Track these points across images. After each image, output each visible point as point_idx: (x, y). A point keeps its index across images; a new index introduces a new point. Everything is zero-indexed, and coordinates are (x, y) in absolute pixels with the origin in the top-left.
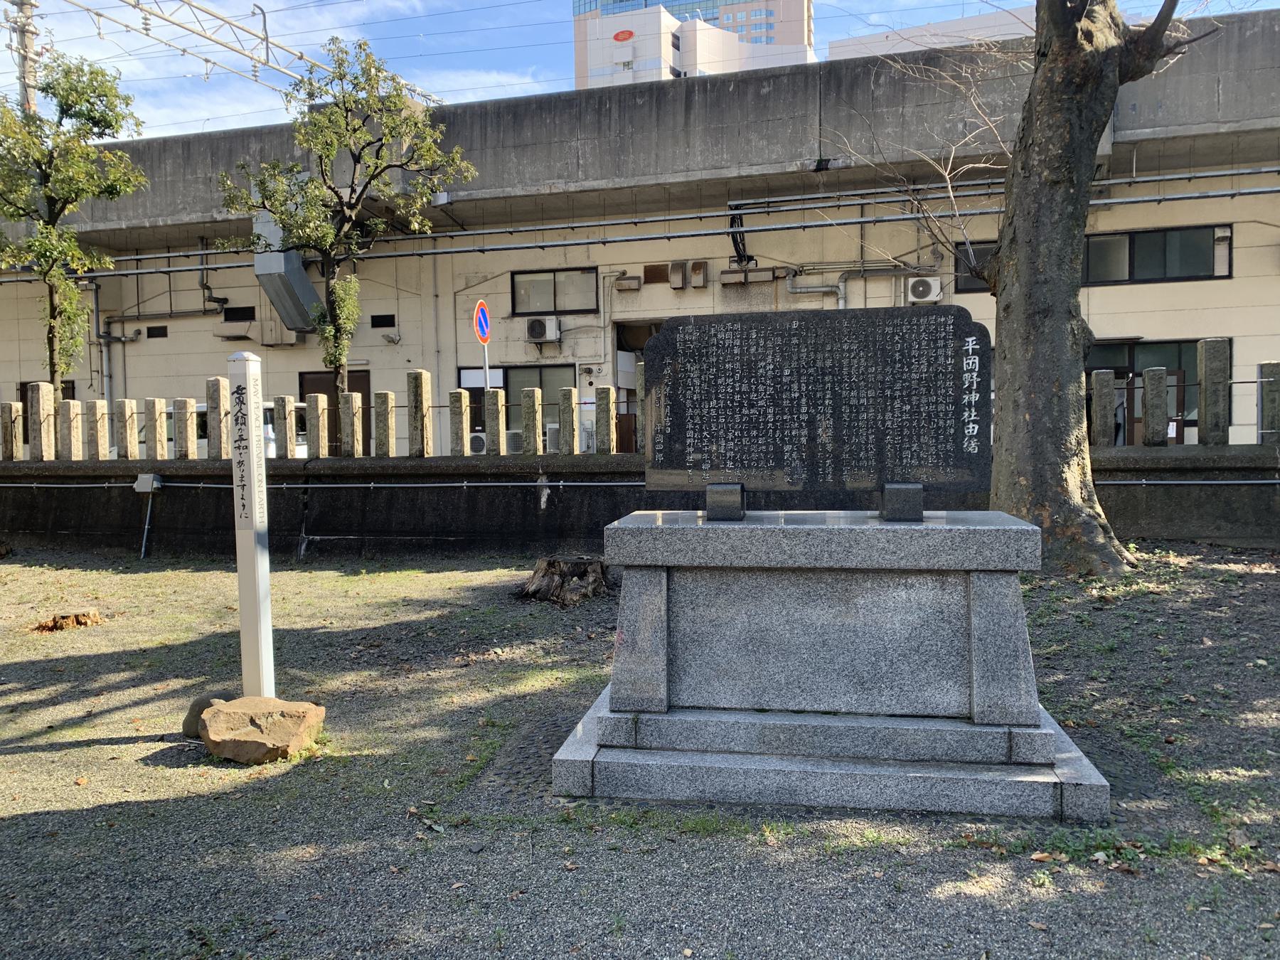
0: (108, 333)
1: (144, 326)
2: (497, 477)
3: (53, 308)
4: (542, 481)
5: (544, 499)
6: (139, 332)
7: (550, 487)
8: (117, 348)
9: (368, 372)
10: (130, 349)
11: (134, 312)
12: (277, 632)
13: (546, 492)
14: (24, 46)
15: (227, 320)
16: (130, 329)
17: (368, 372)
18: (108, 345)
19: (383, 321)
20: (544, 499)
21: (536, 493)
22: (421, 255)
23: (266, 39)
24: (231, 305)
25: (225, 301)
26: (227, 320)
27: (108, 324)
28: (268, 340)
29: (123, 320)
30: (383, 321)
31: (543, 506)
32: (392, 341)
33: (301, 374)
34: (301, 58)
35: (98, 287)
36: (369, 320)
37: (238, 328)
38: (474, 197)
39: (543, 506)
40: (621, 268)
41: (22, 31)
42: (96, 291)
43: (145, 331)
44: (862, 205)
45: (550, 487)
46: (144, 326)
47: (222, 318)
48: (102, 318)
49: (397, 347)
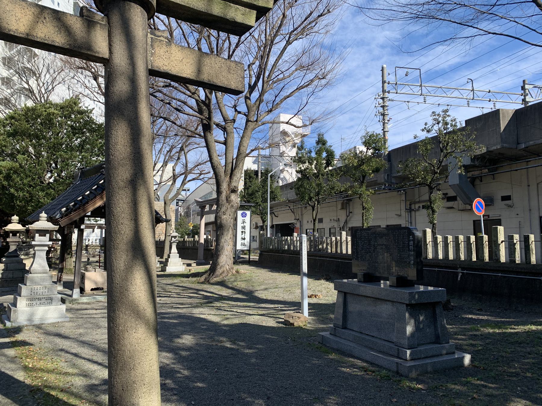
0: (410, 208)
1: (421, 205)
2: (446, 267)
3: (363, 207)
4: (459, 270)
5: (459, 277)
6: (419, 207)
7: (462, 273)
8: (413, 213)
9: (500, 219)
10: (417, 213)
11: (418, 200)
12: (309, 304)
13: (461, 274)
14: (384, 120)
15: (447, 201)
16: (417, 206)
17: (500, 219)
18: (410, 212)
19: (504, 198)
20: (459, 277)
21: (457, 274)
22: (517, 170)
23: (473, 90)
24: (449, 195)
25: (447, 194)
26: (447, 201)
27: (410, 205)
28: (461, 208)
29: (415, 203)
30: (506, 198)
31: (459, 279)
32: (510, 206)
33: (474, 221)
34: (489, 92)
35: (406, 193)
36: (500, 198)
37: (450, 204)
38: (537, 143)
39: (459, 279)
40: (494, 181)
41: (383, 115)
42: (405, 194)
43: (421, 206)
44: (493, 175)
45: (462, 273)
46: (421, 205)
47: (446, 200)
48: (408, 203)
49: (512, 209)
